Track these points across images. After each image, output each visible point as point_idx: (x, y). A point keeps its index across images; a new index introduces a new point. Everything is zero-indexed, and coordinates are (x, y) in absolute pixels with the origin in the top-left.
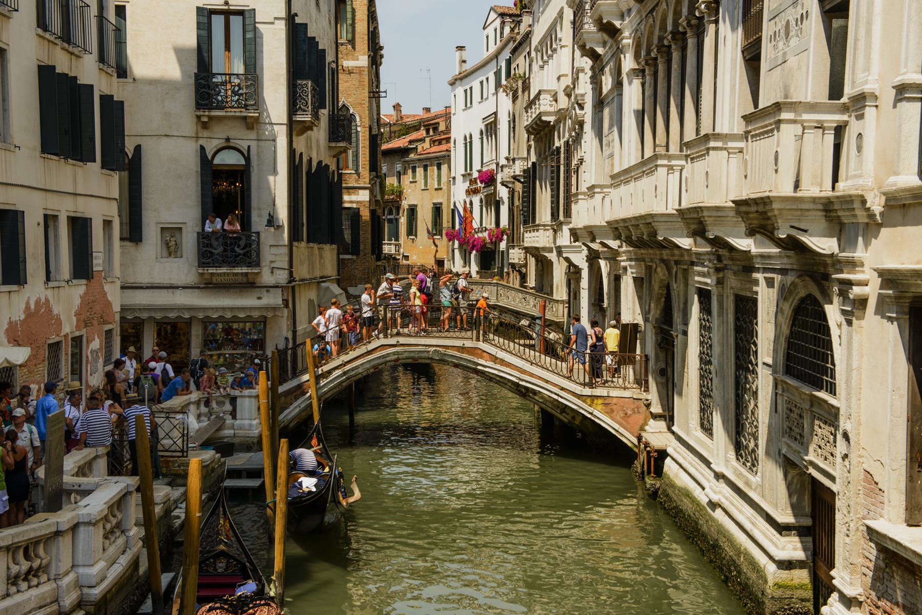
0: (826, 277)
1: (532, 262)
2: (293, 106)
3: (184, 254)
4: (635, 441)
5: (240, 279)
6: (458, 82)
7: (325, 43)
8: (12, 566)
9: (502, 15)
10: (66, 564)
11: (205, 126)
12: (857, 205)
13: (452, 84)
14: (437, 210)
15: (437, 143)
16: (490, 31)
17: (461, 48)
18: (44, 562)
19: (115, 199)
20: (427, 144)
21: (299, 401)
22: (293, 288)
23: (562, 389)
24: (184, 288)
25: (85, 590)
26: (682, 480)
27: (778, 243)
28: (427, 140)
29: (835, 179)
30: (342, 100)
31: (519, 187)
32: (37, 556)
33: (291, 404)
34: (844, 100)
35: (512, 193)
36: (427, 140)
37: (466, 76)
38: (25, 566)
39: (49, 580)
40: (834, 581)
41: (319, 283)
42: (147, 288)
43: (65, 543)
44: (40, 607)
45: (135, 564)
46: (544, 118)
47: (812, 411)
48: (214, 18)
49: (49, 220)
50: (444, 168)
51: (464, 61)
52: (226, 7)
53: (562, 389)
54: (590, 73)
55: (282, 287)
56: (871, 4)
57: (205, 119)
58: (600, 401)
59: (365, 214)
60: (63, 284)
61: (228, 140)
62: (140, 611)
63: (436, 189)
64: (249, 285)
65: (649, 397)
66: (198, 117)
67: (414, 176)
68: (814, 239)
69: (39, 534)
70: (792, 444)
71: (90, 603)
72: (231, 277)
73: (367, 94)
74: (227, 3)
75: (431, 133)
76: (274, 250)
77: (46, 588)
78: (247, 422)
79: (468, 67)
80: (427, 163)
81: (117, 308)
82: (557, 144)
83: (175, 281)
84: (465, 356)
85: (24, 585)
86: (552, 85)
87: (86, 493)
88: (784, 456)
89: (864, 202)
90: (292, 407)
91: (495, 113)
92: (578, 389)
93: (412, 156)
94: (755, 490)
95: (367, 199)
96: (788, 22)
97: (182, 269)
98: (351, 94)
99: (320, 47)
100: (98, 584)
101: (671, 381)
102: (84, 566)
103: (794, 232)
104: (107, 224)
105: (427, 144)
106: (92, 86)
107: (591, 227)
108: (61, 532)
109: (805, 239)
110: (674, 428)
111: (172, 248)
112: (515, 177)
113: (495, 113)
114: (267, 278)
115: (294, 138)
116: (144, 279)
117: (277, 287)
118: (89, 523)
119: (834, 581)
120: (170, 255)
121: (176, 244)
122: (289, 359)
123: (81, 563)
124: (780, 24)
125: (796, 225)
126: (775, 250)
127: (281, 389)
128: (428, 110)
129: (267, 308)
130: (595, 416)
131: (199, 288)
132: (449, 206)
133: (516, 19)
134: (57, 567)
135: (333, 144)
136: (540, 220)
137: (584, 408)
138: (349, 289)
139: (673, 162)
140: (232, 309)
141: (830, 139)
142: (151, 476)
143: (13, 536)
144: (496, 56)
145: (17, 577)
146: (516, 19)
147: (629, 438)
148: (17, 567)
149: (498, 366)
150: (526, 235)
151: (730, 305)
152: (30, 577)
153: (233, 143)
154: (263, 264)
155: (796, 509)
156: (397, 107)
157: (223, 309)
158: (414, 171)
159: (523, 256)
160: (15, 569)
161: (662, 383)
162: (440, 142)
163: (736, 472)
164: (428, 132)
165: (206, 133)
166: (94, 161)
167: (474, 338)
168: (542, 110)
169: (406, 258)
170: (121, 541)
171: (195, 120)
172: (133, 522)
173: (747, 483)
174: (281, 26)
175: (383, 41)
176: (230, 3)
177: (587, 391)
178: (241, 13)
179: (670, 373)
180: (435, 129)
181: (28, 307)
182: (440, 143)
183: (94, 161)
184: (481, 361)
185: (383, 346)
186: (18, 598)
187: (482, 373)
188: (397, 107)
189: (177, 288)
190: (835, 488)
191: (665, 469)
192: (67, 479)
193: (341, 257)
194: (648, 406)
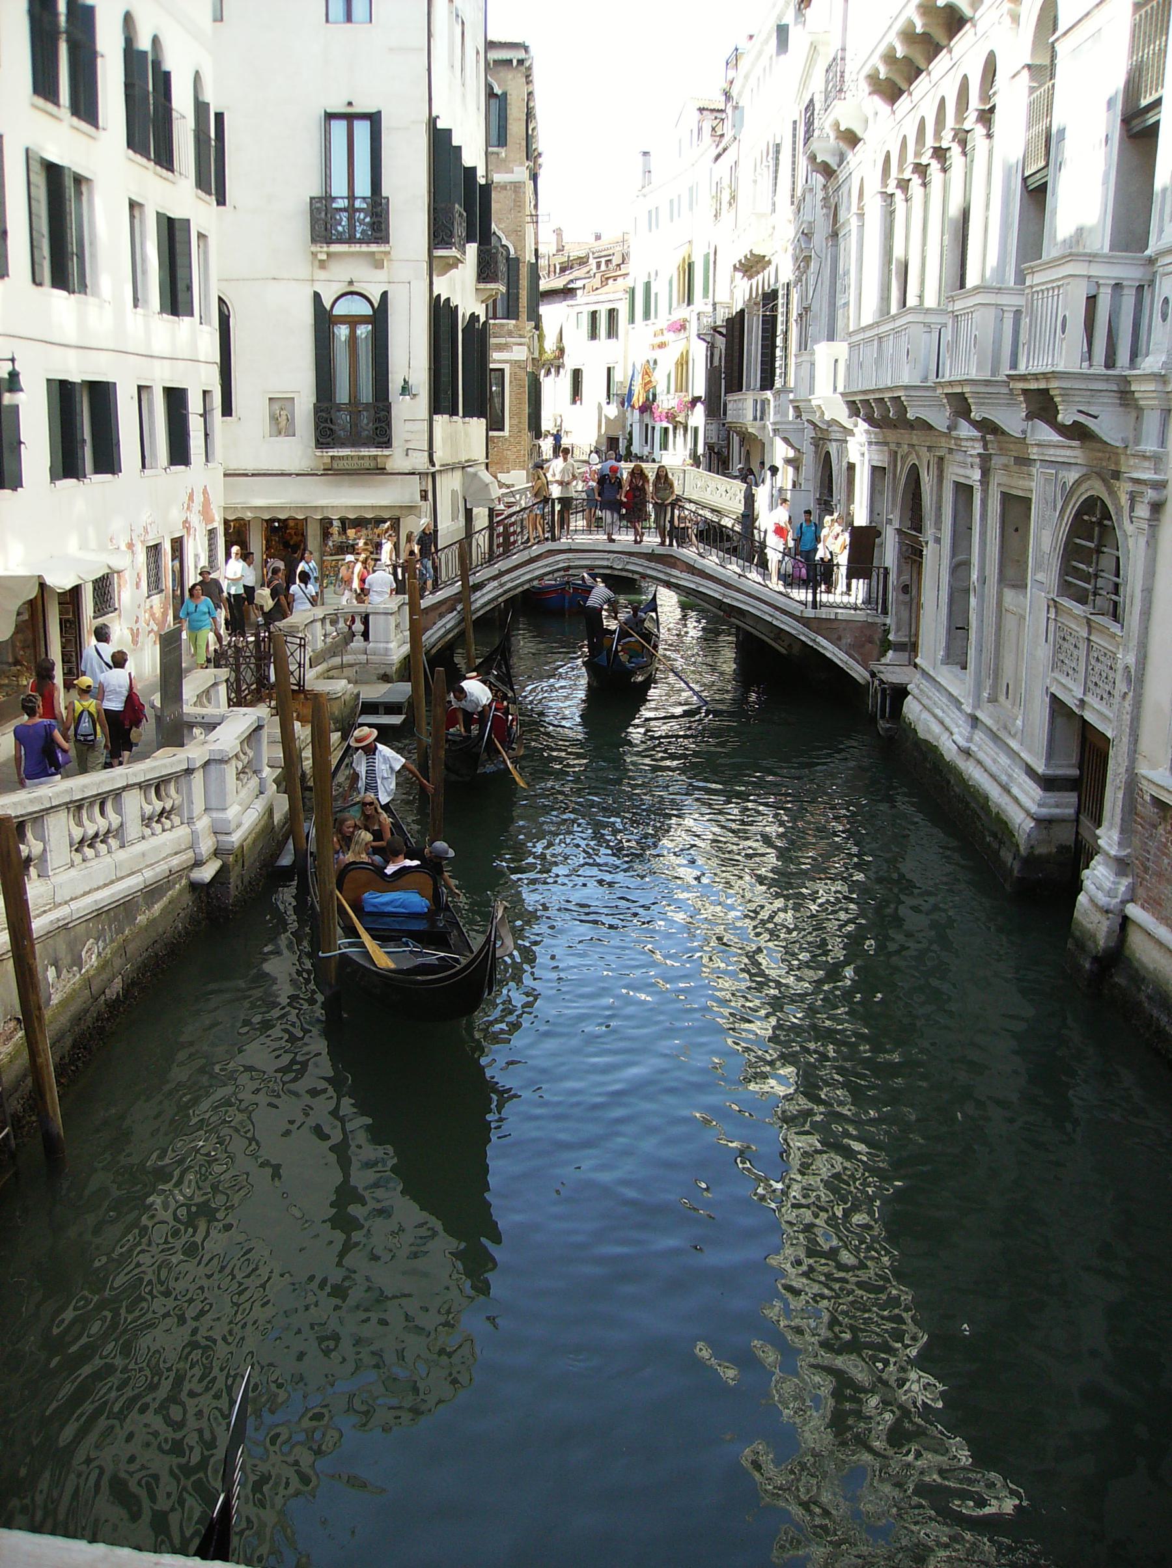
0: (1116, 475)
1: (736, 439)
4: (867, 675)
5: (367, 464)
7: (473, 156)
8: (145, 806)
10: (199, 805)
11: (322, 265)
17: (646, 154)
21: (444, 620)
22: (433, 475)
24: (297, 475)
25: (221, 838)
27: (1062, 429)
28: (598, 276)
31: (721, 342)
34: (1148, 252)
35: (711, 347)
38: (158, 806)
39: (164, 830)
40: (1099, 841)
42: (253, 475)
44: (176, 854)
45: (270, 811)
47: (1089, 640)
54: (820, 195)
57: (324, 257)
61: (351, 283)
62: (278, 864)
65: (888, 621)
66: (314, 254)
70: (1063, 681)
71: (229, 852)
72: (356, 461)
74: (350, 104)
75: (603, 267)
76: (409, 426)
77: (183, 831)
78: (382, 645)
85: (158, 827)
87: (211, 727)
88: (1052, 694)
90: (435, 628)
94: (1013, 736)
97: (297, 450)
99: (455, 143)
100: (234, 831)
101: (915, 601)
103: (1082, 419)
106: (188, 220)
108: (193, 770)
110: (918, 660)
115: (435, 278)
117: (413, 474)
119: (1099, 841)
125: (1081, 408)
126: (1056, 438)
127: (424, 603)
130: (818, 644)
131: (317, 475)
133: (719, 115)
135: (482, 286)
138: (499, 475)
143: (145, 772)
145: (150, 819)
147: (859, 673)
149: (698, 579)
150: (729, 406)
151: (995, 505)
152: (163, 820)
154: (395, 442)
155: (1050, 756)
156: (559, 232)
159: (723, 434)
160: (148, 810)
161: (905, 603)
164: (599, 265)
165: (321, 274)
166: (192, 315)
170: (254, 782)
171: (310, 257)
172: (265, 761)
175: (542, 143)
179: (914, 592)
183: (192, 315)
185: (551, 553)
186: (153, 841)
188: (559, 232)
189: (290, 475)
190: (1109, 735)
191: (905, 709)
192: (187, 709)
193: (491, 433)
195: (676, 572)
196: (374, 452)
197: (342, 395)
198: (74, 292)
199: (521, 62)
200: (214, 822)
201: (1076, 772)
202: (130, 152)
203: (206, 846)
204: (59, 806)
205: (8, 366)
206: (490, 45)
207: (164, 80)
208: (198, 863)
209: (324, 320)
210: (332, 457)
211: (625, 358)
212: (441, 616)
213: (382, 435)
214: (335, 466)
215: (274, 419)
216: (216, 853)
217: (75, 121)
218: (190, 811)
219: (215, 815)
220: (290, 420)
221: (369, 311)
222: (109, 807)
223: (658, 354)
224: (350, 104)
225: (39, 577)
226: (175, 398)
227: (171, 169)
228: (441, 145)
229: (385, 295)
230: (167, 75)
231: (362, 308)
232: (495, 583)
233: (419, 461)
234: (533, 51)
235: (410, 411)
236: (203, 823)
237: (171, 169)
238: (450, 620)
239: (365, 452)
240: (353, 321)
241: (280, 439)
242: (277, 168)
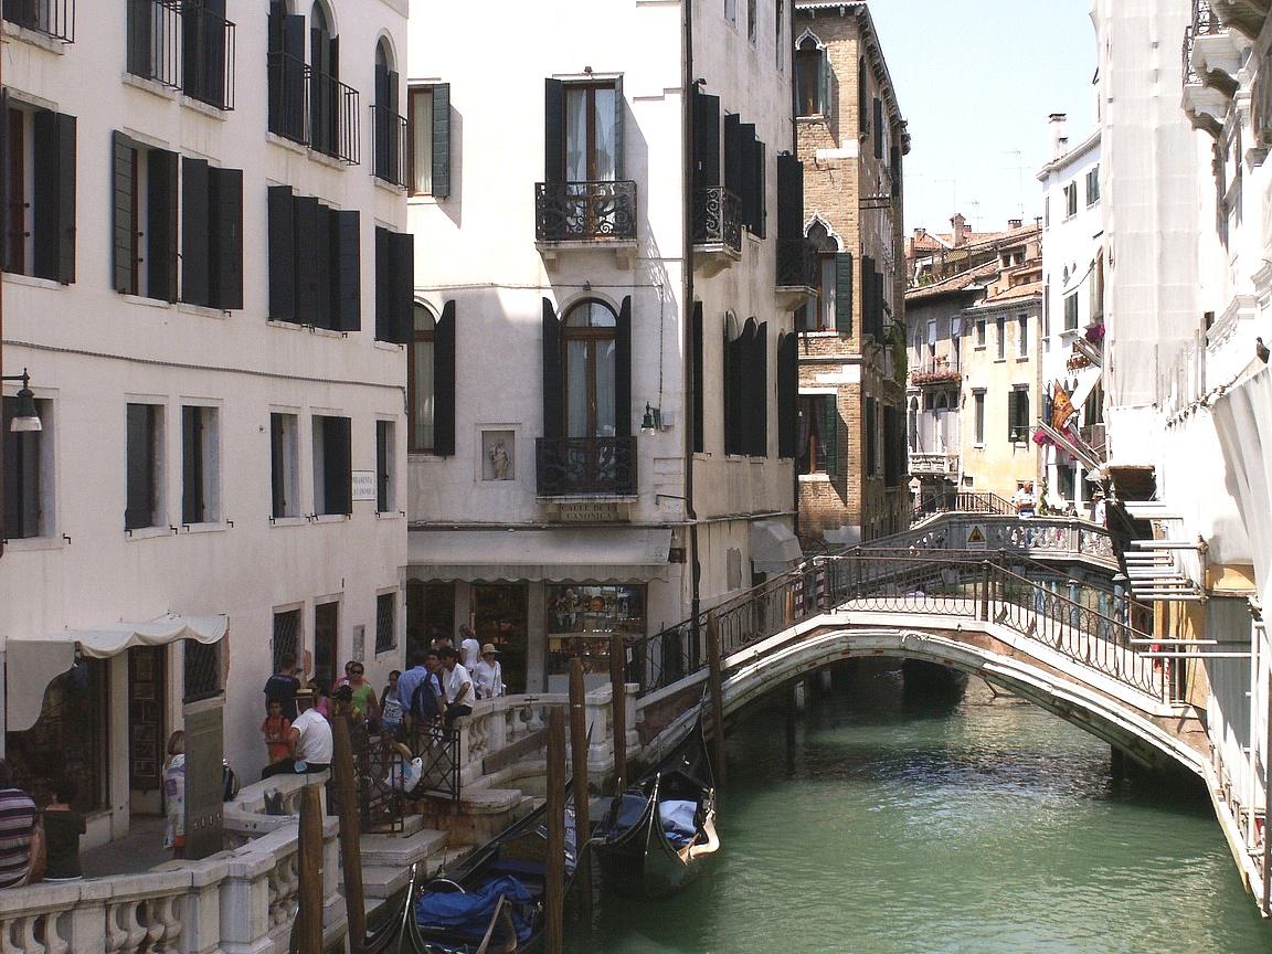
2: (696, 228)
3: (517, 474)
6: (1053, 176)
13: (1044, 179)
15: (1021, 281)
17: (1057, 117)
18: (172, 931)
19: (402, 388)
20: (1003, 284)
22: (694, 528)
24: (516, 528)
28: (1005, 276)
30: (811, 212)
32: (160, 921)
33: (671, 721)
36: (1005, 276)
37: (1066, 165)
41: (750, 521)
42: (461, 528)
43: (209, 902)
49: (280, 425)
50: (1032, 322)
51: (1063, 140)
52: (589, 78)
55: (673, 527)
56: (48, 2)
59: (850, 411)
60: (304, 520)
61: (587, 287)
63: (1019, 361)
64: (619, 526)
67: (982, 339)
69: (166, 886)
73: (856, 204)
74: (588, 70)
76: (660, 467)
80: (1001, 316)
83: (502, 518)
84: (961, 644)
93: (978, 304)
95: (857, 379)
97: (514, 500)
98: (832, 206)
102: (237, 943)
104: (384, 428)
105: (1003, 284)
108: (199, 888)
111: (500, 464)
114: (648, 512)
116: (457, 515)
117: (665, 527)
118: (242, 880)
120: (496, 477)
121: (506, 458)
122: (686, 651)
123: (233, 939)
128: (1017, 223)
131: (539, 528)
134: (193, 939)
135: (783, 289)
148: (124, 935)
153: (596, 292)
154: (642, 489)
158: (982, 330)
162: (1026, 279)
164: (1007, 263)
167: (979, 616)
169: (969, 480)
174: (676, 104)
176: (594, 70)
180: (1019, 256)
182: (1027, 281)
187: (997, 677)
188: (1252, 317)
189: (506, 528)
196: (613, 498)
197: (576, 427)
198: (174, 301)
202: (273, 136)
204: (94, 901)
207: (328, 49)
211: (1039, 379)
212: (680, 712)
213: (626, 480)
214: (564, 518)
217: (188, 100)
220: (508, 460)
221: (612, 322)
222: (51, 930)
224: (588, 70)
225: (76, 643)
226: (334, 432)
227: (333, 152)
228: (700, 109)
229: (627, 300)
230: (335, 43)
233: (675, 510)
235: (660, 453)
237: (333, 152)
238: (688, 719)
239: (600, 498)
241: (496, 482)
242: (503, 155)
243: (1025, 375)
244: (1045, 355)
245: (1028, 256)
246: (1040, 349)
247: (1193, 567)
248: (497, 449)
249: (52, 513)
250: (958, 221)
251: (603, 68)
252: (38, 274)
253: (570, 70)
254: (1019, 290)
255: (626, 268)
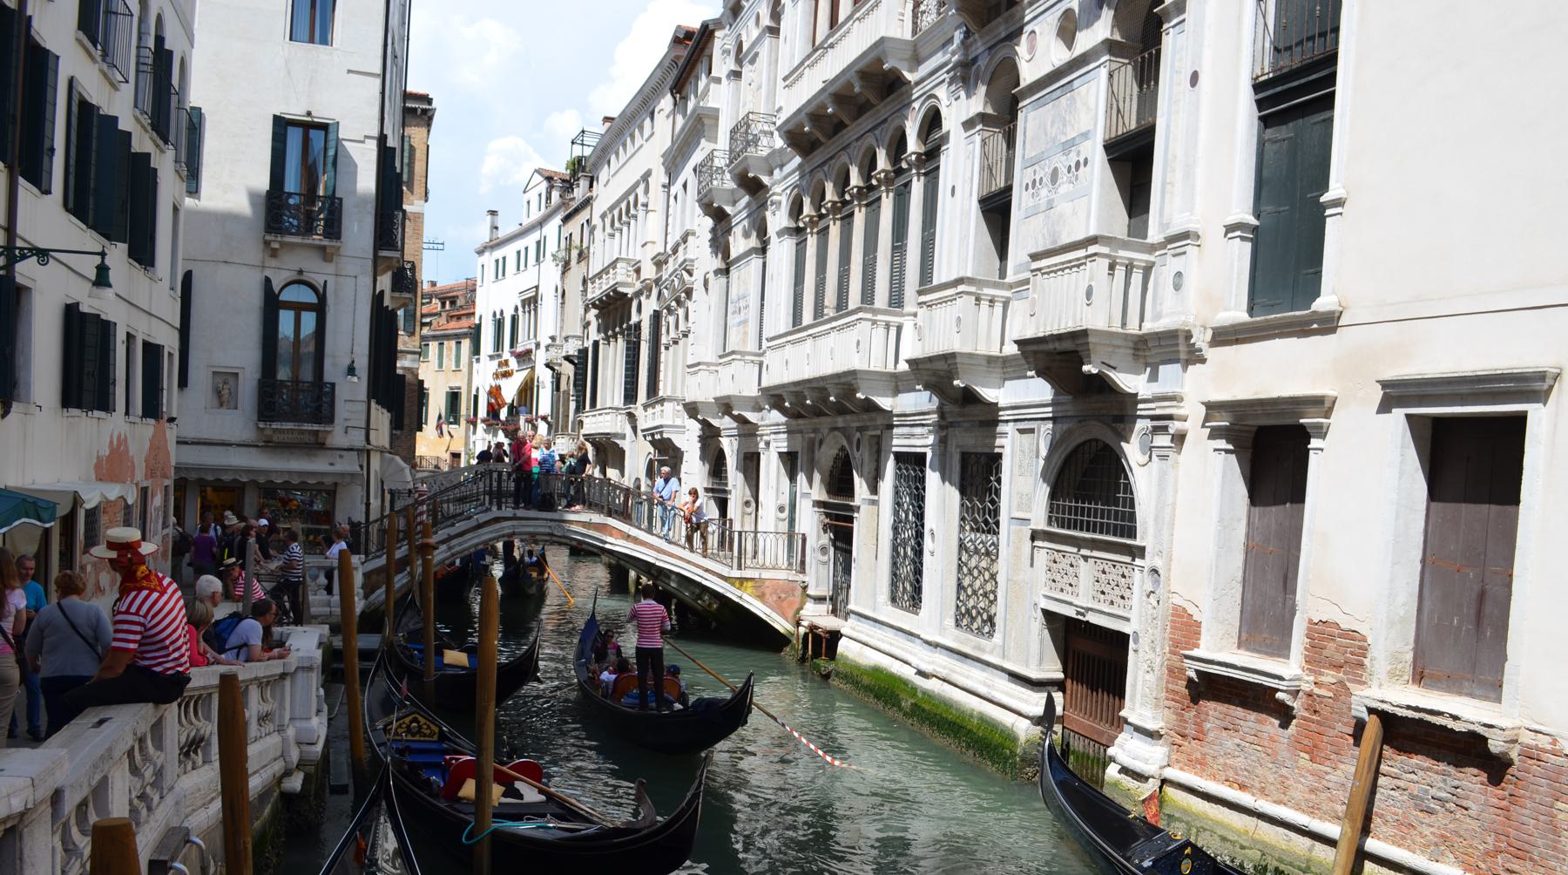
1: (589, 447)
5: (306, 438)
9: (549, 179)
11: (274, 254)
12: (1181, 340)
14: (454, 398)
16: (533, 196)
17: (493, 213)
20: (443, 320)
22: (368, 452)
23: (707, 570)
26: (869, 658)
29: (1142, 320)
35: (557, 378)
46: (621, 289)
48: (291, 130)
53: (707, 570)
57: (276, 246)
58: (750, 584)
61: (301, 272)
64: (317, 445)
65: (806, 579)
66: (267, 243)
68: (1121, 376)
74: (309, 114)
76: (349, 406)
79: (502, 234)
81: (173, 463)
82: (634, 319)
83: (226, 437)
86: (636, 253)
89: (1188, 335)
91: (537, 287)
92: (725, 571)
96: (1055, 171)
97: (237, 423)
107: (729, 397)
109: (1112, 374)
111: (225, 397)
112: (567, 358)
113: (537, 287)
120: (221, 405)
124: (1044, 172)
129: (342, 475)
132: (469, 391)
135: (397, 295)
136: (604, 401)
137: (732, 593)
139: (880, 317)
140: (300, 473)
141: (757, 368)
142: (355, 627)
144: (541, 223)
146: (568, 185)
147: (781, 624)
153: (305, 277)
157: (290, 472)
163: (957, 639)
164: (443, 305)
165: (273, 263)
168: (619, 279)
173: (979, 648)
174: (373, 146)
176: (615, 114)
177: (736, 573)
178: (324, 127)
180: (453, 303)
181: (111, 442)
184: (609, 539)
185: (497, 520)
191: (840, 650)
194: (805, 588)
195: (609, 539)
196: (316, 427)
199: (425, 111)
200: (298, 731)
201: (1061, 676)
203: (295, 756)
205: (98, 260)
206: (407, 96)
208: (287, 773)
209: (272, 304)
210: (275, 430)
215: (218, 393)
216: (300, 765)
218: (282, 717)
219: (298, 724)
220: (234, 395)
223: (503, 382)
224: (309, 114)
231: (309, 297)
232: (443, 547)
233: (357, 439)
234: (434, 105)
236: (291, 732)
239: (307, 427)
240: (298, 308)
241: (222, 410)
243: (459, 382)
244: (475, 365)
245: (459, 303)
246: (471, 365)
247: (689, 499)
248: (224, 388)
249: (28, 385)
250: (1339, 203)
251: (322, 114)
252: (1260, 118)
253: (295, 110)
254: (453, 324)
255: (331, 261)
